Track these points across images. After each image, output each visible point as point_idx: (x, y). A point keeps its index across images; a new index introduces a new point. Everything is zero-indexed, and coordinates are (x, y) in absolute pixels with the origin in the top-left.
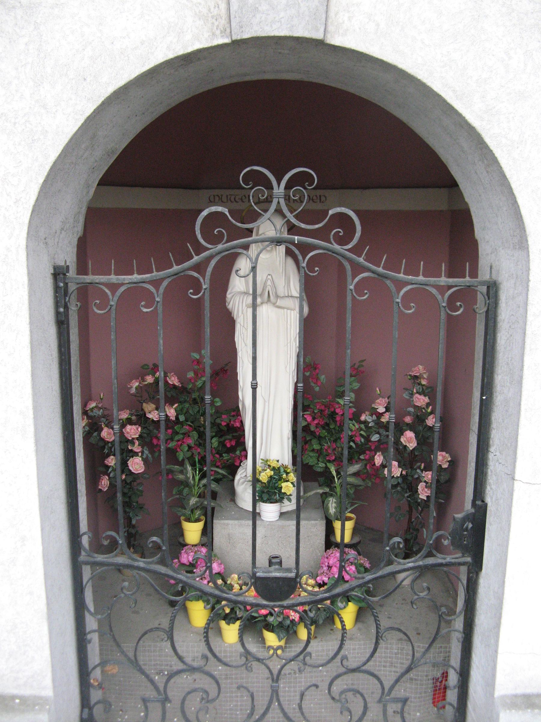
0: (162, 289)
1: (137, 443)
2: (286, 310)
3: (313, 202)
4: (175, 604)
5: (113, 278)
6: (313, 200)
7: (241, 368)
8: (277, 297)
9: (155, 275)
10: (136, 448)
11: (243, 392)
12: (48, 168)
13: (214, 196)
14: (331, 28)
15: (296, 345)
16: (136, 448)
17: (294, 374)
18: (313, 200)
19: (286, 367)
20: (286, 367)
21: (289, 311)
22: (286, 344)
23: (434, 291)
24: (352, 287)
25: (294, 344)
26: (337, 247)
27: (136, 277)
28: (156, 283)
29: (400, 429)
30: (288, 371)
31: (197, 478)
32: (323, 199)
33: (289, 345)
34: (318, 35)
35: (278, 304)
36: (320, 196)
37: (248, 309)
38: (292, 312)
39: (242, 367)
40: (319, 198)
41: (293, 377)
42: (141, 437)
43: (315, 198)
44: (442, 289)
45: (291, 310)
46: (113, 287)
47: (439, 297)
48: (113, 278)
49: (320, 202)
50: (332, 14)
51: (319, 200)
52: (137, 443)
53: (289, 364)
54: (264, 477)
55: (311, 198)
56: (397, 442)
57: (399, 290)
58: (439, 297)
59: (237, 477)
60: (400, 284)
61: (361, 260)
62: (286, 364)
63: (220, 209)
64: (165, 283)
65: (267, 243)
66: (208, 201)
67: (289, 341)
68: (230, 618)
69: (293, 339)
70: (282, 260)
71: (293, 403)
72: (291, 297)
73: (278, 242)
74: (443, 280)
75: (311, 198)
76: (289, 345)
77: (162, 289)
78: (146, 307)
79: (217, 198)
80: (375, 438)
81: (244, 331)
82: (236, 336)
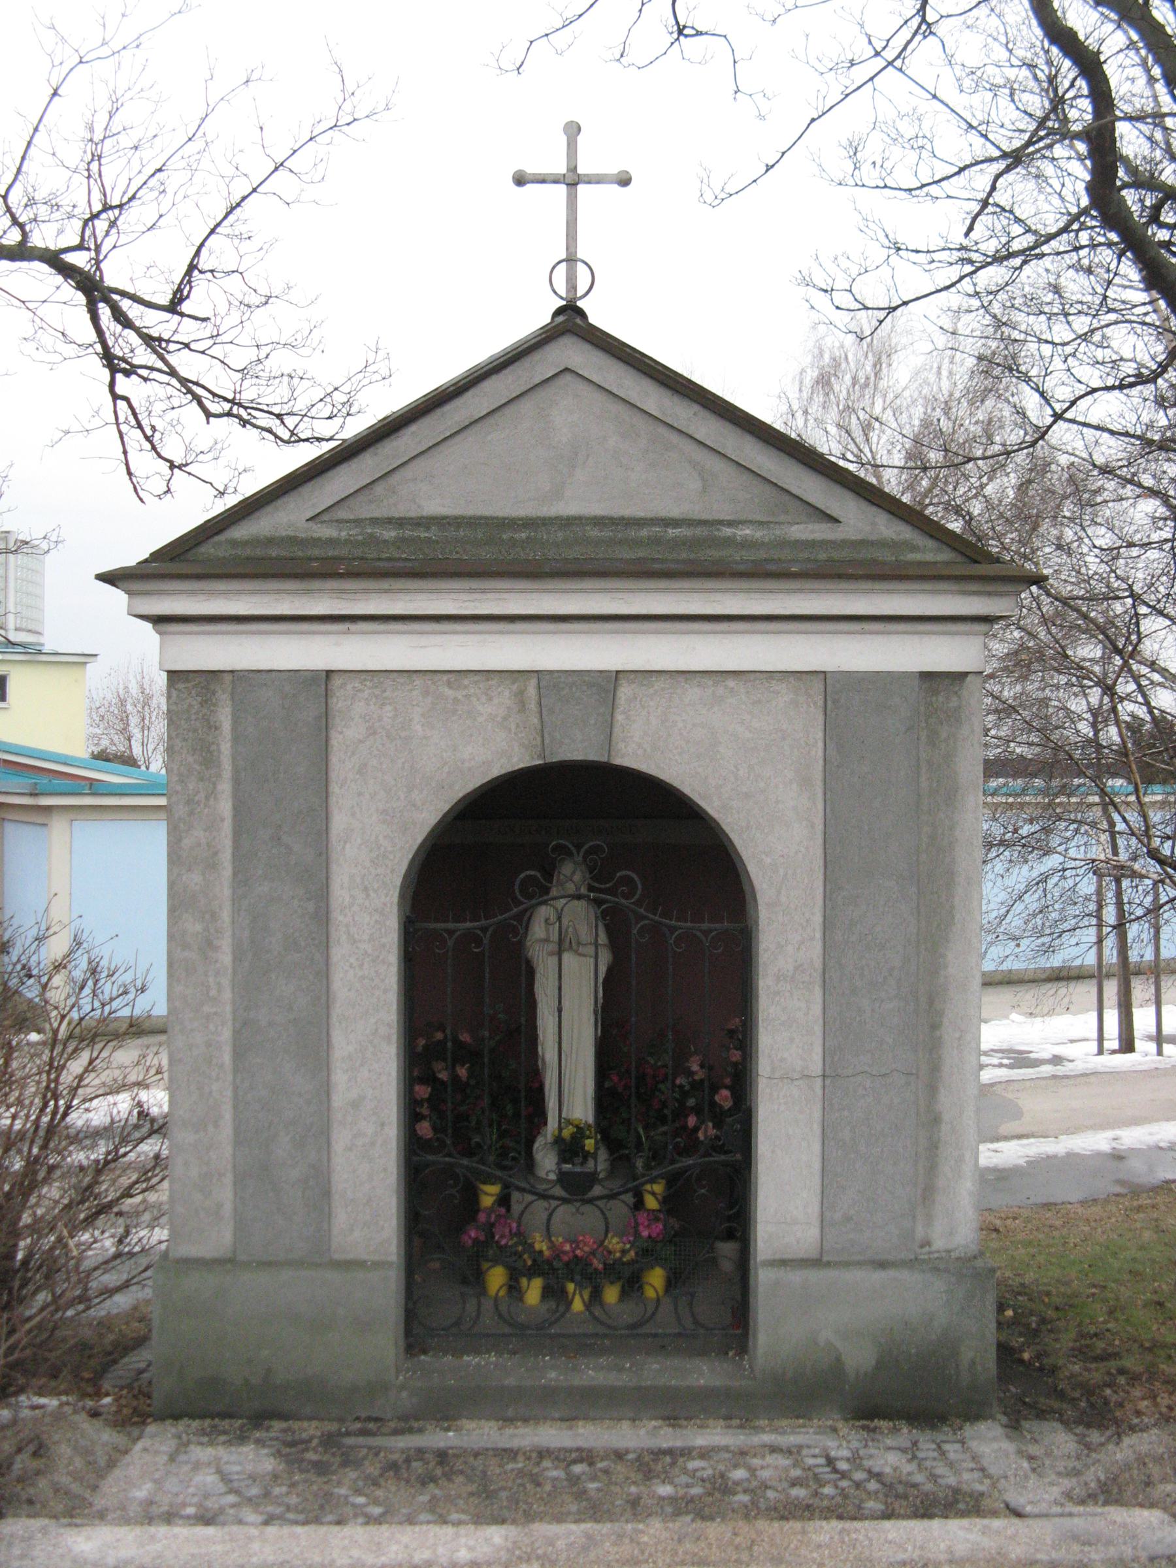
0: (488, 934)
1: (426, 1105)
4: (537, 1085)
5: (451, 926)
8: (579, 943)
9: (483, 922)
10: (425, 1111)
12: (416, 847)
14: (613, 753)
16: (425, 1111)
23: (699, 934)
24: (635, 932)
26: (623, 901)
27: (468, 925)
28: (484, 929)
29: (715, 1089)
31: (494, 1137)
34: (604, 759)
42: (429, 1100)
44: (706, 933)
46: (451, 932)
47: (703, 938)
48: (451, 926)
50: (613, 743)
52: (426, 1105)
54: (566, 1133)
56: (713, 1104)
57: (672, 933)
58: (703, 938)
59: (536, 1145)
60: (672, 929)
61: (642, 910)
63: (532, 873)
64: (491, 929)
68: (532, 1273)
70: (400, 564)
73: (579, 897)
74: (705, 926)
77: (488, 934)
78: (476, 947)
80: (691, 1102)
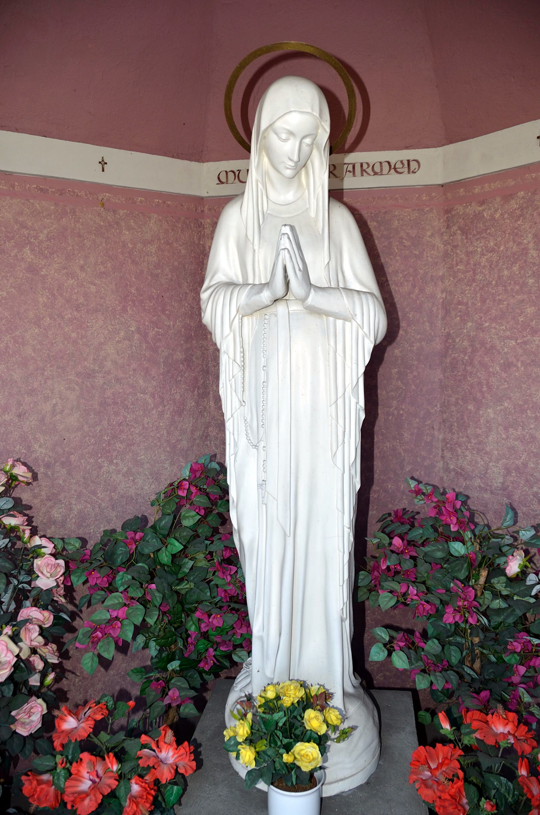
2: (331, 319)
3: (397, 172)
6: (395, 169)
7: (233, 458)
11: (239, 510)
13: (226, 172)
15: (357, 403)
17: (353, 472)
18: (395, 169)
19: (334, 455)
20: (334, 455)
21: (339, 323)
22: (333, 400)
25: (354, 401)
30: (339, 464)
32: (413, 165)
33: (340, 401)
35: (310, 301)
36: (409, 161)
37: (245, 319)
38: (348, 324)
39: (236, 454)
40: (406, 165)
41: (351, 478)
43: (399, 165)
45: (345, 319)
49: (409, 172)
51: (406, 170)
53: (340, 448)
55: (393, 167)
62: (334, 448)
65: (479, 771)
66: (218, 182)
67: (340, 393)
69: (349, 390)
71: (352, 539)
72: (345, 289)
75: (393, 167)
76: (340, 401)
79: (231, 175)
81: (235, 373)
82: (221, 385)
